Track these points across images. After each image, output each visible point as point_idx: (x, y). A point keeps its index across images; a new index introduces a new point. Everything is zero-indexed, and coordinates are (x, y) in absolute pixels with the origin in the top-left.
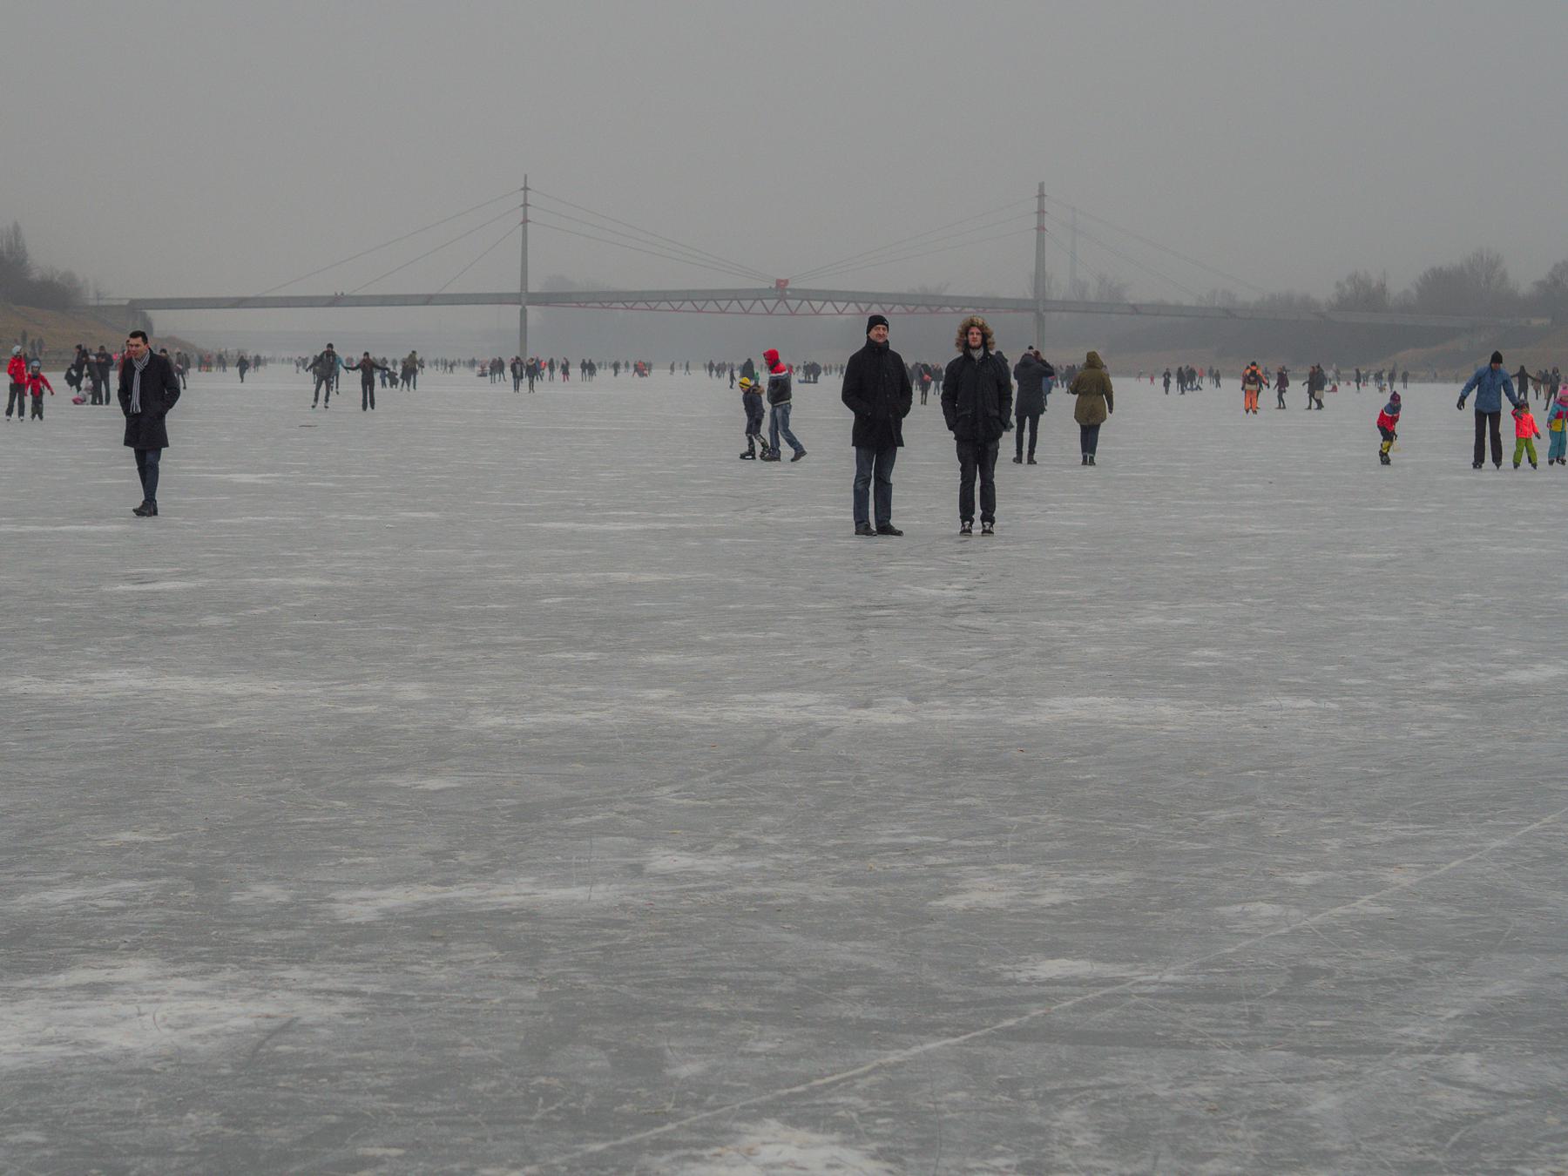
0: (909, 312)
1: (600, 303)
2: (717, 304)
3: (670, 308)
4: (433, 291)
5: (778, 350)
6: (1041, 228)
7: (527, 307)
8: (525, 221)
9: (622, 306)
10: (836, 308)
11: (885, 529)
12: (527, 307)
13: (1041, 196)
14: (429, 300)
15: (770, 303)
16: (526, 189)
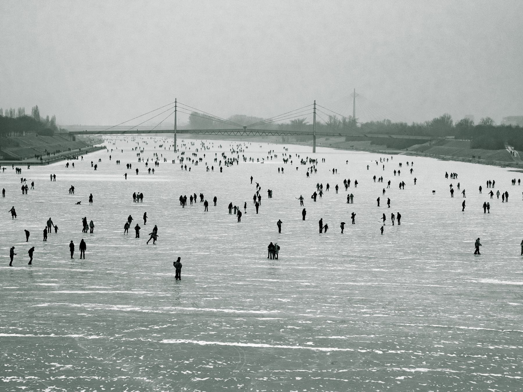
4: (151, 130)
6: (315, 113)
7: (176, 134)
8: (176, 111)
11: (354, 224)
12: (176, 134)
13: (315, 104)
14: (322, 153)
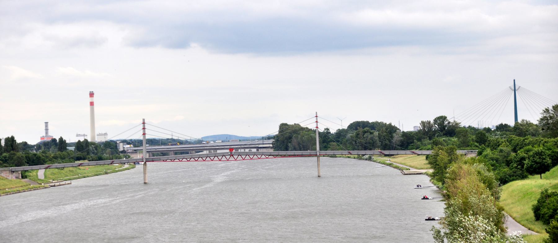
0: (188, 161)
1: (178, 159)
2: (218, 158)
3: (194, 160)
5: (14, 136)
9: (178, 160)
10: (218, 159)
13: (144, 123)
15: (228, 157)
16: (317, 116)
